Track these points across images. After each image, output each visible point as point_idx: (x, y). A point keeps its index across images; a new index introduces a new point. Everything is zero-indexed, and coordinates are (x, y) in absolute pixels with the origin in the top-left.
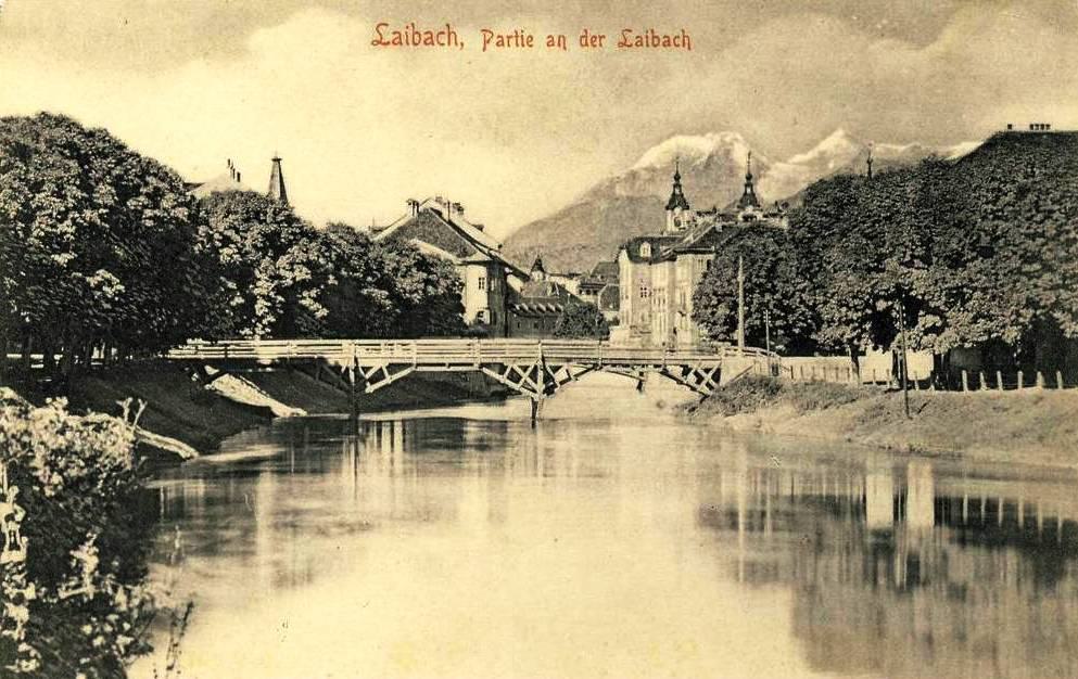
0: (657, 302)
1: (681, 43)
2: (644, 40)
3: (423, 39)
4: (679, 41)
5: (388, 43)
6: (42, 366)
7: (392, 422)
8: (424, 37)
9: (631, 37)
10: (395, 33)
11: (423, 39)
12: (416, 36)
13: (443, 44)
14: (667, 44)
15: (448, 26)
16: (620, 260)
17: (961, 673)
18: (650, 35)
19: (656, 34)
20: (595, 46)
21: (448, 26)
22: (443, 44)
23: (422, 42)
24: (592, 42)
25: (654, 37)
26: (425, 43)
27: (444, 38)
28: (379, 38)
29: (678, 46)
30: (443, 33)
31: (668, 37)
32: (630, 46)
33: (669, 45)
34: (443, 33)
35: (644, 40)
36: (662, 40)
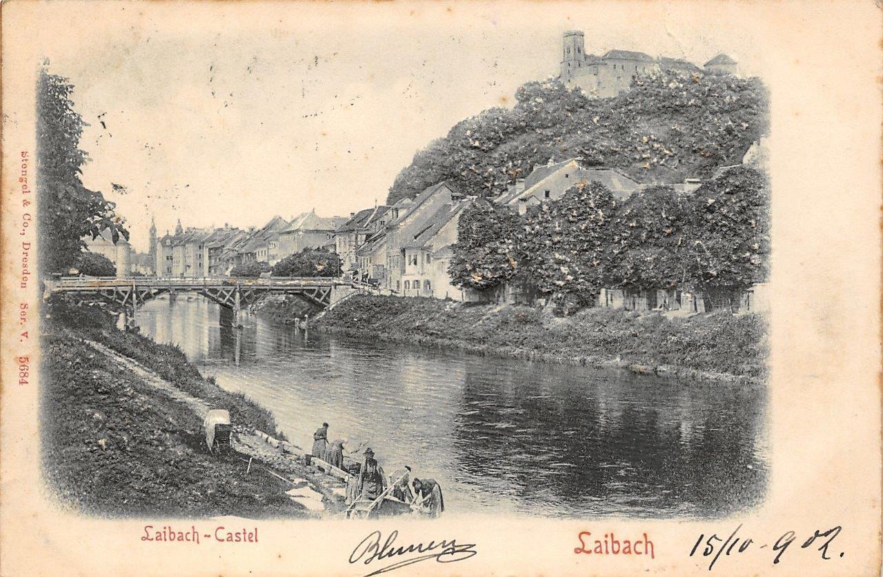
0: (260, 254)
1: (191, 538)
2: (163, 535)
3: (621, 549)
4: (190, 537)
5: (152, 539)
6: (687, 180)
7: (136, 286)
8: (177, 536)
9: (152, 534)
10: (157, 533)
11: (621, 549)
12: (172, 535)
13: (640, 553)
14: (627, 551)
15: (645, 535)
16: (92, 178)
17: (678, 371)
18: (167, 530)
19: (172, 531)
20: (252, 541)
21: (645, 535)
22: (640, 553)
23: (176, 539)
24: (249, 538)
25: (171, 533)
26: (624, 552)
27: (640, 548)
28: (146, 536)
29: (252, 541)
30: (640, 542)
31: (629, 542)
32: (589, 552)
33: (182, 539)
34: (640, 542)
35: (163, 535)
36: (177, 536)
